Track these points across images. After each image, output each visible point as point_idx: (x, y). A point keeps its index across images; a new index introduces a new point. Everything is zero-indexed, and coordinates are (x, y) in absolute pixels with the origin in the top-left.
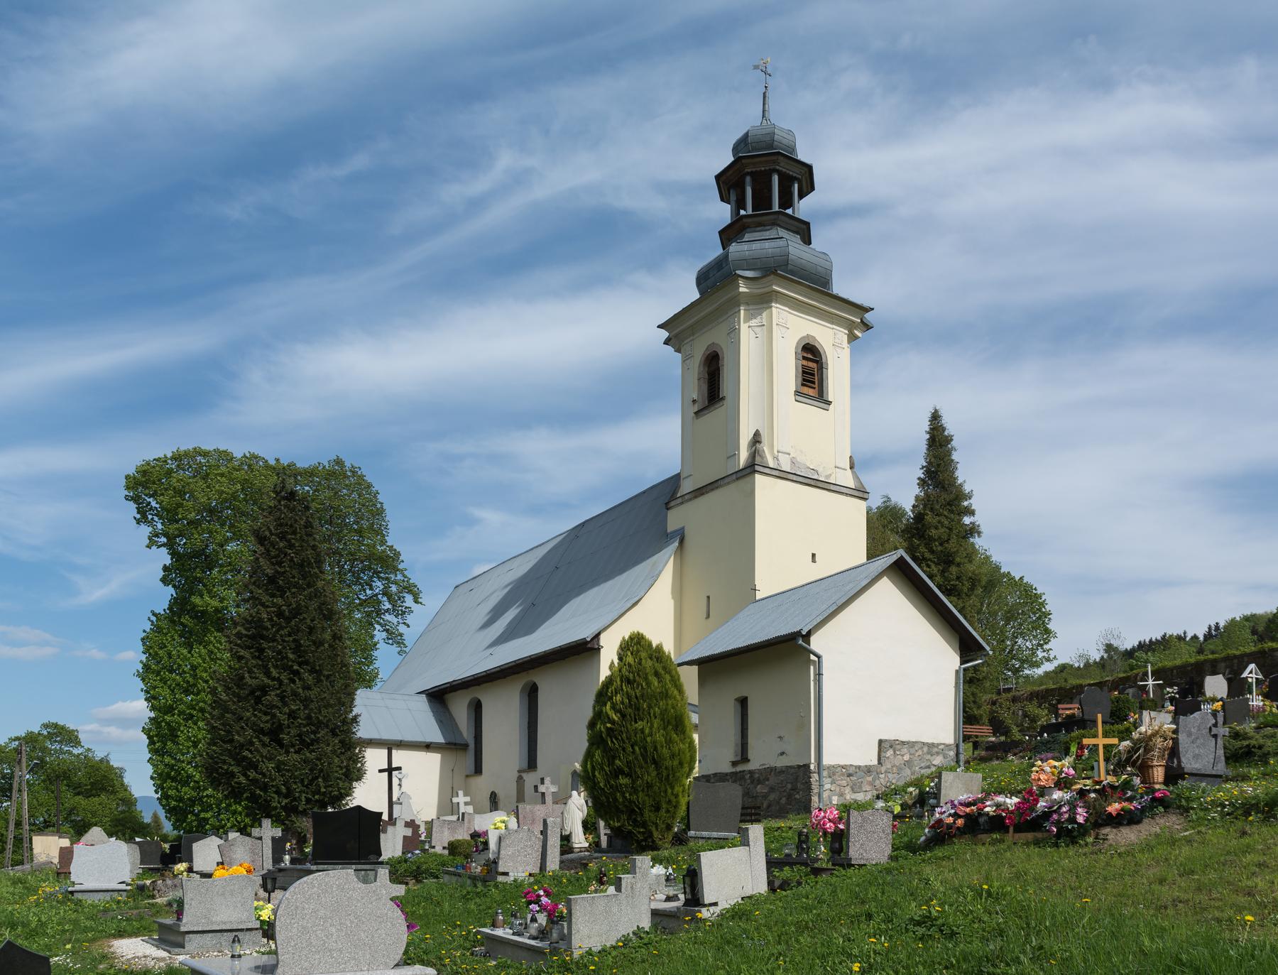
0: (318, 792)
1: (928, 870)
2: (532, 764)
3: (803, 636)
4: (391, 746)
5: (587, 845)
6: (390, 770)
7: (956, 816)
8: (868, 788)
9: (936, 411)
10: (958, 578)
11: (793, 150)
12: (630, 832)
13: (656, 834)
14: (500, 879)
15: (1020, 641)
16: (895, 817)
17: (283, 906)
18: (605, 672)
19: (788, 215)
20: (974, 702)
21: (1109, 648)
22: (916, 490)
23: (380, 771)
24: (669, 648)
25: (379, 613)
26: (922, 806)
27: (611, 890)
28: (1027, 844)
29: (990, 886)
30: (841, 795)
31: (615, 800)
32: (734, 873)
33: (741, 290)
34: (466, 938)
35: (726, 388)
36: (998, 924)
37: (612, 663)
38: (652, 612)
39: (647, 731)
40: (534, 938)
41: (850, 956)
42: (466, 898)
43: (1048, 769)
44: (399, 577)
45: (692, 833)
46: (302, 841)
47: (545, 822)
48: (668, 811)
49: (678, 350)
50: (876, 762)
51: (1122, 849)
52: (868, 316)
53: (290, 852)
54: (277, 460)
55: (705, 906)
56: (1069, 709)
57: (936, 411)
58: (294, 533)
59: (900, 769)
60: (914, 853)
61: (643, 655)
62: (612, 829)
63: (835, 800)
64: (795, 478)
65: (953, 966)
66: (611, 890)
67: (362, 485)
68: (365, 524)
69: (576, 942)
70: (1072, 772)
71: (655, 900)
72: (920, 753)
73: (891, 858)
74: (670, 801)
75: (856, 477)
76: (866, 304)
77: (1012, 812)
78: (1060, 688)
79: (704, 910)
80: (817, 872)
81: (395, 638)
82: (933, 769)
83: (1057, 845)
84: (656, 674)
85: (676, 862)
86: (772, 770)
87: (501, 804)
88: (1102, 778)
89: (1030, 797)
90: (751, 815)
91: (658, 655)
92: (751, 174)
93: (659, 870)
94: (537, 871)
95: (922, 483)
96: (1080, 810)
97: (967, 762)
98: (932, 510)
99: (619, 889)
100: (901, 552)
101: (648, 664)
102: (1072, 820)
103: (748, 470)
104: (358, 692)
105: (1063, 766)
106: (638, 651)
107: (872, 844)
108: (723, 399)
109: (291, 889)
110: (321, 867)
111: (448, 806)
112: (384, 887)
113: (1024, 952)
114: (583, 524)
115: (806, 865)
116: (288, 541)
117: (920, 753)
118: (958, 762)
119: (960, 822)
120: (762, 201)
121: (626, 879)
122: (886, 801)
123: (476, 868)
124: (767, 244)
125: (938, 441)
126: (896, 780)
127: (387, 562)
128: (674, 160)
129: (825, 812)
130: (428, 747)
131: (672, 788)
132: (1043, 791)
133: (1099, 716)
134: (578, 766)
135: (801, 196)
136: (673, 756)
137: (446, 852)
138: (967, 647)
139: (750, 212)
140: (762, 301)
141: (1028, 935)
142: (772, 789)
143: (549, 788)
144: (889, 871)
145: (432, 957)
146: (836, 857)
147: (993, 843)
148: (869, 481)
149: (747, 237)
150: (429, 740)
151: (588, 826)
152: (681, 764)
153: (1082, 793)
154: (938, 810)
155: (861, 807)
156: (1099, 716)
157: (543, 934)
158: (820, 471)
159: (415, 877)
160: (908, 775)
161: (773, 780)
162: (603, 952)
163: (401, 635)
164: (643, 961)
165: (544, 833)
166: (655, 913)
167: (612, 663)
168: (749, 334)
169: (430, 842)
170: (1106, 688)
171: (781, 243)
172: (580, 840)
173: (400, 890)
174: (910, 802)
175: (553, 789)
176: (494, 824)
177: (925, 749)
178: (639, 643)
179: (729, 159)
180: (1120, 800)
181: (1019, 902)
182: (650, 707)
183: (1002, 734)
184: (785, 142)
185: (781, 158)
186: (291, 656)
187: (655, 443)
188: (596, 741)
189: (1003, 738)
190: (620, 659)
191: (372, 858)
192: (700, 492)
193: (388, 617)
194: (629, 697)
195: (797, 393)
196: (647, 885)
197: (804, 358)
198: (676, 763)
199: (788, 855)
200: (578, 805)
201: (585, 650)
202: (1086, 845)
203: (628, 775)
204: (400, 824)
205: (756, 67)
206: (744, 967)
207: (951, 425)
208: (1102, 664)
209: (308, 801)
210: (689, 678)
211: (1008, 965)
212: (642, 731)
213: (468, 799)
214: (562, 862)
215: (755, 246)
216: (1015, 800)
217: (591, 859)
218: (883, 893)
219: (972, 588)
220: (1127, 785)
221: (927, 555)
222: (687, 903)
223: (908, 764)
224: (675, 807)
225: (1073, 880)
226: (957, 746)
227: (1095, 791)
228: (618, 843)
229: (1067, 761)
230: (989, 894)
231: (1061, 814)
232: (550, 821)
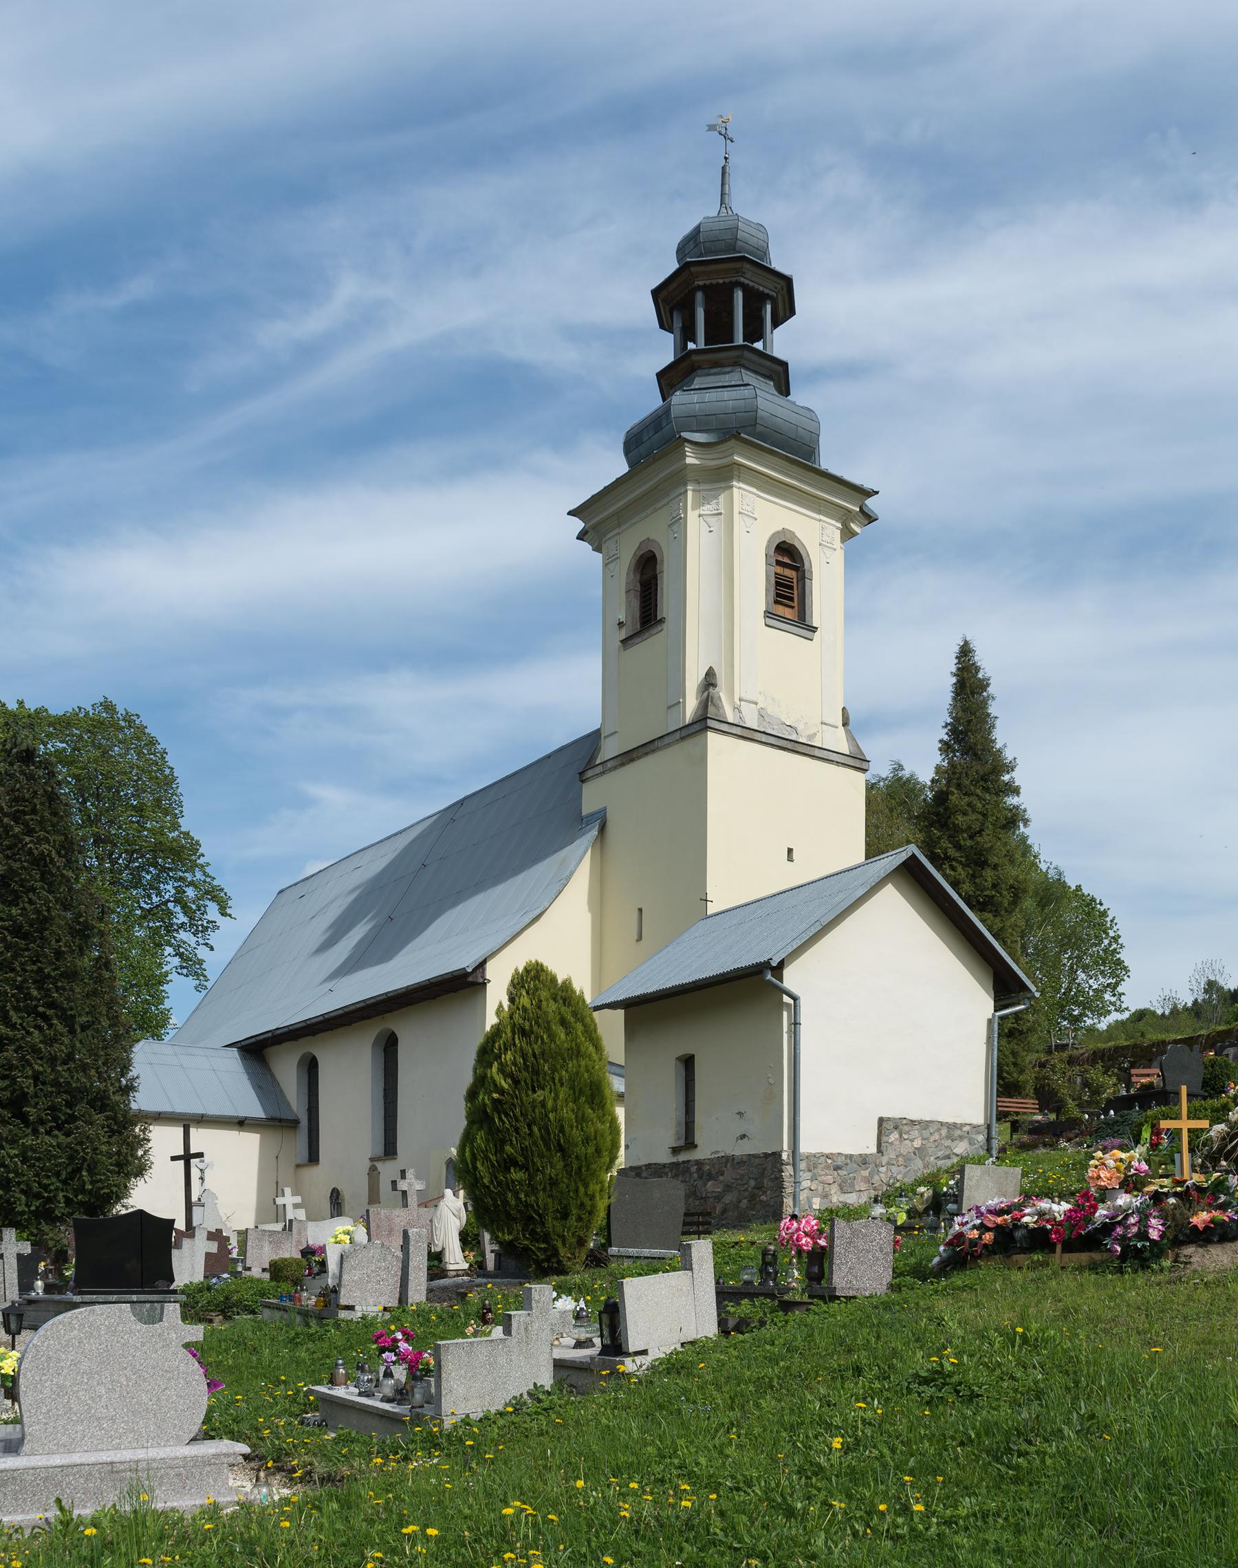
0: (82, 1190)
1: (942, 1305)
2: (390, 1149)
3: (773, 969)
4: (188, 1122)
5: (466, 1266)
6: (187, 1157)
7: (982, 1228)
8: (863, 1186)
9: (966, 643)
10: (994, 886)
11: (765, 253)
12: (526, 1249)
13: (563, 1252)
14: (343, 1315)
15: (1082, 976)
16: (898, 1229)
17: (29, 1356)
18: (491, 1020)
19: (756, 351)
20: (1015, 1064)
21: (1211, 986)
22: (937, 758)
23: (174, 1158)
24: (583, 985)
25: (170, 929)
26: (937, 1214)
27: (498, 1332)
28: (1080, 1269)
29: (1027, 1329)
30: (825, 1196)
31: (505, 1202)
32: (670, 1309)
33: (689, 461)
34: (294, 1400)
35: (666, 607)
36: (1036, 1382)
37: (501, 1006)
38: (560, 933)
39: (550, 1104)
40: (387, 1400)
41: (829, 1427)
42: (293, 1342)
43: (1111, 1163)
44: (199, 875)
45: (613, 1250)
46: (60, 1258)
47: (405, 1233)
48: (580, 1219)
49: (598, 549)
50: (873, 1150)
51: (1210, 1277)
52: (871, 503)
53: (44, 1276)
54: (21, 703)
55: (628, 1354)
56: (1146, 1077)
57: (966, 643)
58: (34, 811)
59: (907, 1160)
60: (924, 1280)
61: (544, 994)
62: (500, 1243)
63: (817, 1204)
64: (764, 738)
65: (972, 1441)
66: (498, 1332)
67: (144, 742)
68: (148, 798)
69: (447, 1405)
70: (1144, 1167)
71: (560, 1345)
72: (936, 1136)
73: (894, 1288)
74: (582, 1205)
75: (851, 738)
76: (868, 485)
77: (1060, 1223)
78: (1135, 1046)
79: (628, 1361)
80: (787, 1306)
81: (191, 965)
82: (955, 1160)
83: (1120, 1271)
84: (563, 1022)
85: (591, 1291)
86: (728, 1160)
87: (346, 1208)
88: (1186, 1176)
89: (1086, 1201)
90: (698, 1224)
91: (565, 994)
92: (704, 288)
93: (567, 1304)
94: (395, 1303)
95: (946, 747)
96: (1153, 1222)
97: (1003, 1150)
98: (959, 786)
99: (507, 1331)
100: (913, 849)
101: (551, 1007)
102: (1143, 1235)
103: (697, 727)
104: (137, 1048)
105: (1132, 1158)
106: (536, 989)
107: (863, 1268)
108: (662, 621)
109: (41, 1331)
110: (87, 1298)
111: (270, 1209)
112: (176, 1329)
113: (1068, 1422)
114: (461, 802)
115: (772, 1296)
116: (26, 824)
117: (936, 1136)
118: (989, 1150)
119: (988, 1237)
120: (719, 329)
121: (518, 1316)
122: (888, 1205)
123: (309, 1300)
124: (726, 394)
125: (969, 686)
126: (902, 1175)
127: (182, 854)
128: (592, 303)
129: (799, 1222)
130: (241, 1123)
131: (586, 1186)
132: (1105, 1194)
133: (1184, 1089)
134: (454, 1151)
135: (776, 323)
136: (586, 1141)
137: (267, 1276)
138: (1005, 987)
139: (702, 346)
140: (721, 477)
141: (1076, 1399)
142: (728, 1188)
143: (412, 1184)
144: (887, 1306)
145: (245, 1428)
146: (815, 1285)
147: (1034, 1266)
148: (868, 750)
149: (698, 382)
150: (242, 1113)
151: (468, 1239)
152: (598, 1151)
153: (1157, 1198)
154: (958, 1219)
155: (851, 1214)
156: (1184, 1089)
157: (401, 1395)
158: (800, 727)
159: (223, 1312)
160: (918, 1168)
161: (729, 1175)
162: (485, 1420)
163: (201, 962)
164: (541, 1434)
165: (405, 1248)
166: (559, 1365)
167: (501, 1006)
169: (243, 1261)
170: (1197, 1047)
172: (456, 1259)
173: (196, 1332)
174: (921, 1208)
175: (419, 1186)
176: (333, 1236)
177: (944, 1132)
178: (537, 977)
179: (674, 266)
180: (1210, 1207)
181: (1065, 1351)
182: (554, 1069)
183: (1051, 1111)
184: (753, 241)
185: (747, 266)
186: (35, 993)
187: (567, 692)
188: (479, 1117)
189: (1053, 1117)
190: (512, 1000)
191: (161, 1284)
192: (628, 757)
193: (183, 935)
194: (524, 1056)
195: (768, 614)
196: (550, 1323)
197: (778, 563)
198: (591, 1150)
199: (748, 1283)
200: (453, 1211)
201: (463, 985)
202: (1162, 1270)
203: (523, 1167)
204: (201, 1236)
205: (712, 128)
206: (681, 1442)
207: (987, 662)
208: (1196, 1010)
209: (68, 1202)
210: (611, 1029)
211: (1046, 1440)
212: (543, 1104)
213: (298, 1199)
214: (430, 1291)
215: (709, 396)
216: (1065, 1206)
217: (470, 1287)
218: (878, 1338)
219: (1016, 900)
220: (1220, 1186)
221: (952, 852)
222: (605, 1350)
223: (920, 1152)
224: (590, 1213)
225: (1141, 1321)
226: (989, 1127)
227: (1176, 1195)
228: (511, 1263)
229: (1138, 1152)
230: (1025, 1340)
231: (1128, 1227)
232: (412, 1232)
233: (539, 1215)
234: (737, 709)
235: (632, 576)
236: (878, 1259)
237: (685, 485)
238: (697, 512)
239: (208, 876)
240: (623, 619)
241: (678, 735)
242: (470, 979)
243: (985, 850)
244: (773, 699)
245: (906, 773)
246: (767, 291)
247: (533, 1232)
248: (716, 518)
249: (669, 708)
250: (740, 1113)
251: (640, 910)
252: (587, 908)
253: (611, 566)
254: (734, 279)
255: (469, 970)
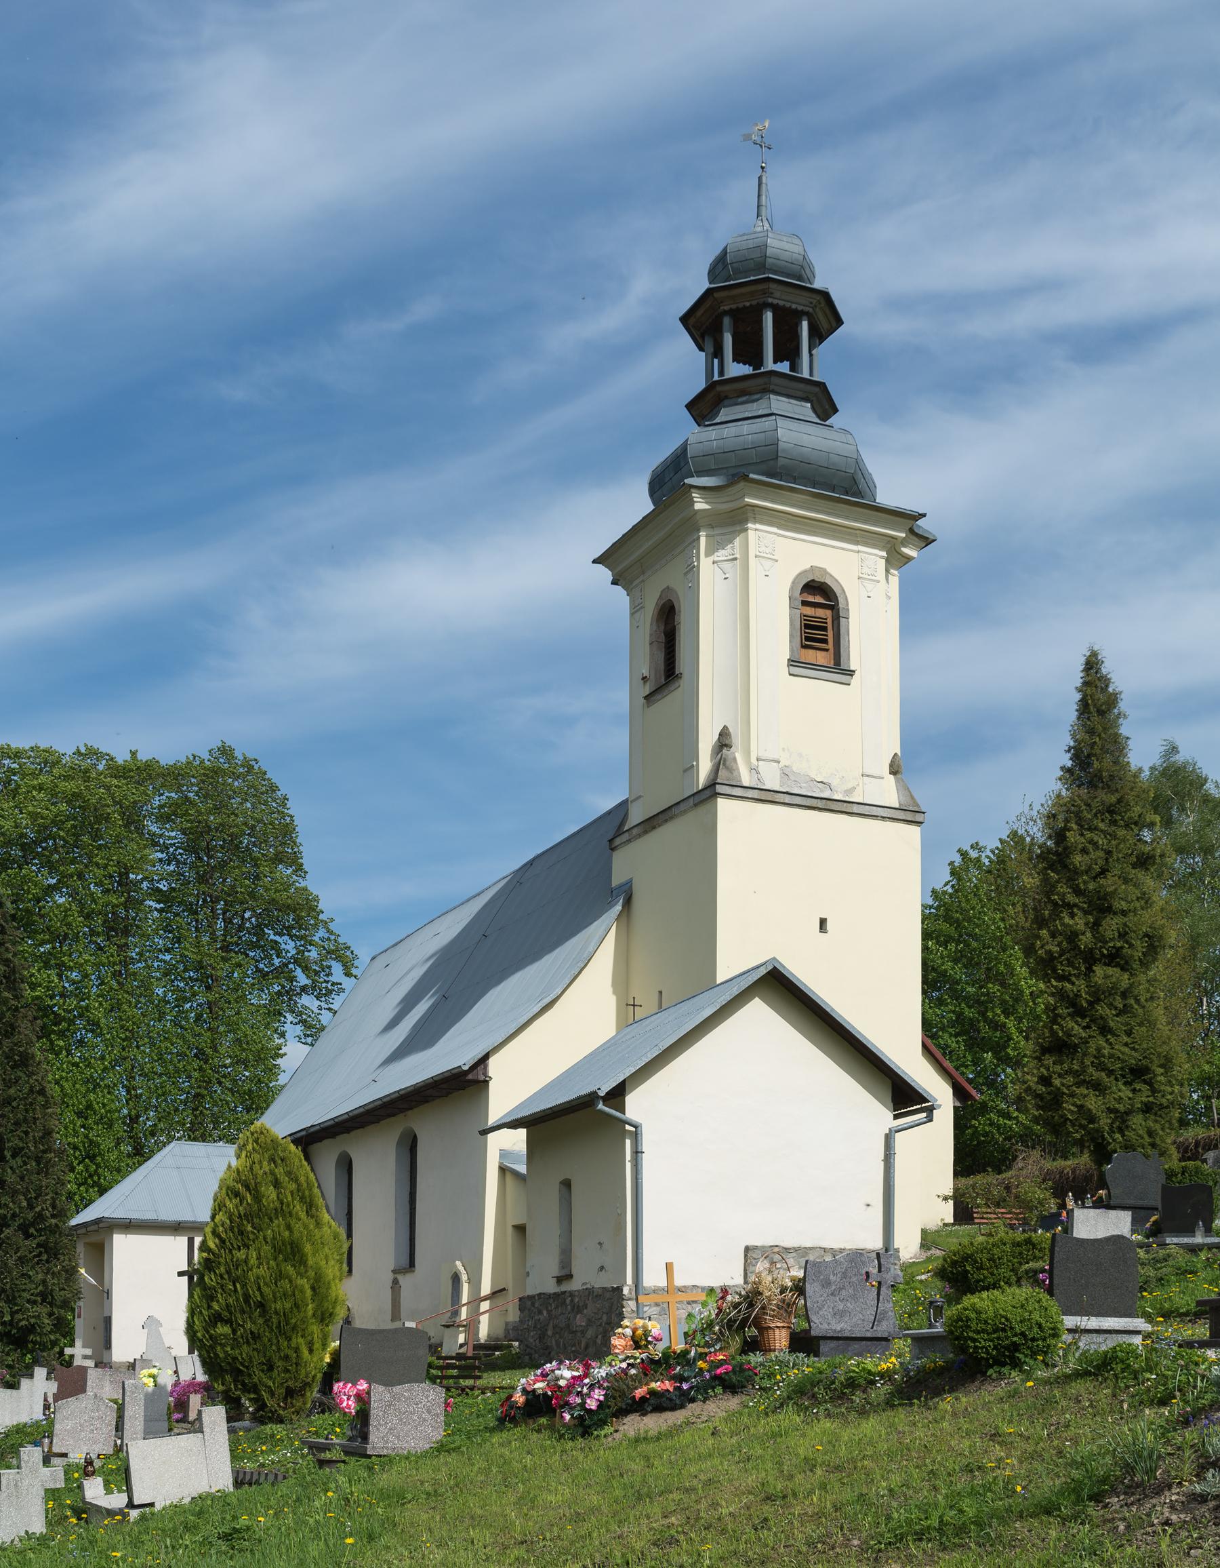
9: (1094, 654)
10: (1123, 935)
20: (1153, 1145)
25: (290, 994)
31: (216, 1355)
33: (697, 506)
35: (682, 665)
64: (787, 799)
74: (287, 1357)
75: (903, 787)
92: (731, 313)
103: (708, 793)
114: (531, 863)
124: (746, 427)
127: (299, 913)
140: (733, 522)
168: (712, 573)
171: (766, 424)
185: (773, 286)
195: (792, 662)
197: (804, 603)
203: (228, 1322)
207: (1122, 677)
221: (1071, 898)
233: (247, 1367)
234: (754, 770)
235: (655, 628)
236: (424, 1420)
237: (699, 531)
238: (711, 559)
239: (332, 933)
240: (646, 674)
241: (691, 801)
242: (470, 1077)
243: (1107, 894)
244: (800, 755)
245: (1179, 758)
246: (800, 308)
247: (244, 1384)
248: (730, 564)
249: (685, 771)
250: (600, 1244)
251: (660, 992)
252: (610, 989)
253: (638, 614)
254: (761, 301)
255: (466, 1068)
